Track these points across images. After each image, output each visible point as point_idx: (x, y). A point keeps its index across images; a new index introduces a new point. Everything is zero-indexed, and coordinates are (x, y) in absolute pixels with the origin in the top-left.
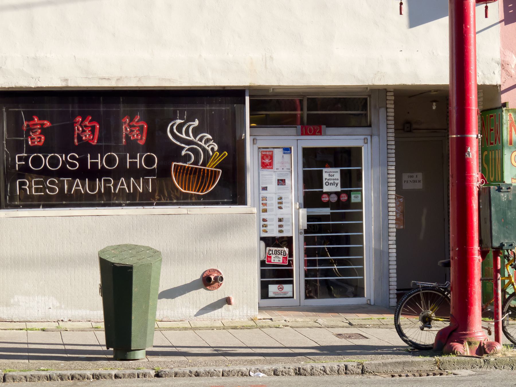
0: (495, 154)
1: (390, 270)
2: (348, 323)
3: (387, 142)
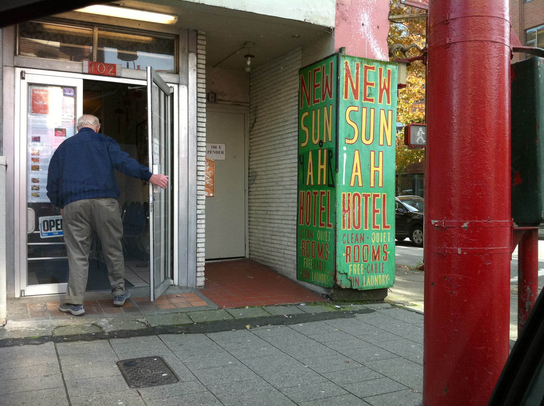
1: (198, 244)
3: (197, 94)
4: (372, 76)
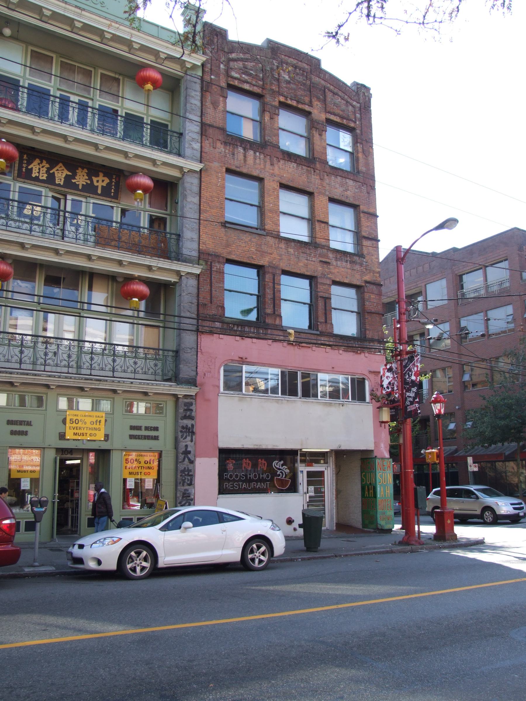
0: (371, 475)
4: (385, 463)
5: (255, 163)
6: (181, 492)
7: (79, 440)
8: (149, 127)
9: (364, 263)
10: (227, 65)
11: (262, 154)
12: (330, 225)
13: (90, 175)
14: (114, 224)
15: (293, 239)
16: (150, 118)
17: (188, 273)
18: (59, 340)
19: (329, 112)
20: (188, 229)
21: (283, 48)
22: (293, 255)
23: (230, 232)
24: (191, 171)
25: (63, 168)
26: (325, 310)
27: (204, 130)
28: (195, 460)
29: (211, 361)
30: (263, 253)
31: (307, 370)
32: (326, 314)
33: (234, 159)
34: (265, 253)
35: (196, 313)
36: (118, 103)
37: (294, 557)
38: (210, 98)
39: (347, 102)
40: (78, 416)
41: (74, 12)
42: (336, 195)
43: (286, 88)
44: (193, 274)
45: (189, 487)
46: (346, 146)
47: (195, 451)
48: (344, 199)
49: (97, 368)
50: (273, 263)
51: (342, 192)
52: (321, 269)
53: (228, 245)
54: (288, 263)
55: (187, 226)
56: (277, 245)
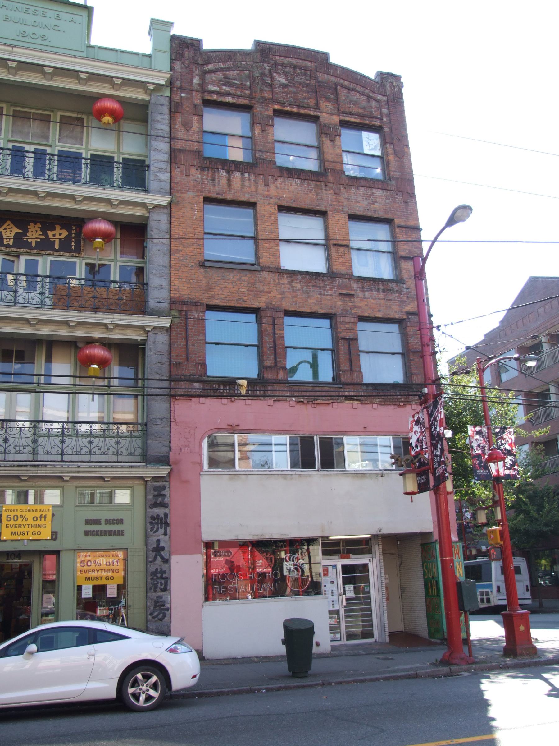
2: (310, 363)
5: (243, 186)
6: (152, 599)
7: (19, 540)
8: (88, 162)
9: (405, 290)
10: (203, 78)
11: (253, 175)
12: (353, 249)
13: (44, 230)
14: (112, 284)
15: (299, 271)
16: (90, 153)
17: (155, 328)
18: (49, 424)
19: (343, 113)
20: (155, 275)
21: (277, 48)
22: (299, 290)
23: (211, 272)
24: (156, 207)
25: (12, 225)
26: (350, 354)
27: (173, 156)
28: (170, 557)
29: (189, 433)
30: (257, 293)
31: (334, 433)
32: (350, 360)
33: (214, 185)
34: (261, 292)
35: (168, 375)
36: (82, 145)
37: (255, 687)
38: (180, 119)
39: (369, 97)
40: (16, 511)
41: (5, 50)
42: (357, 211)
43: (283, 92)
44: (162, 328)
45: (164, 593)
46: (372, 149)
47: (170, 547)
48: (369, 214)
49: (125, 452)
50: (271, 304)
51: (366, 205)
52: (340, 303)
53: (209, 288)
54: (293, 302)
55: (154, 271)
56: (277, 281)
